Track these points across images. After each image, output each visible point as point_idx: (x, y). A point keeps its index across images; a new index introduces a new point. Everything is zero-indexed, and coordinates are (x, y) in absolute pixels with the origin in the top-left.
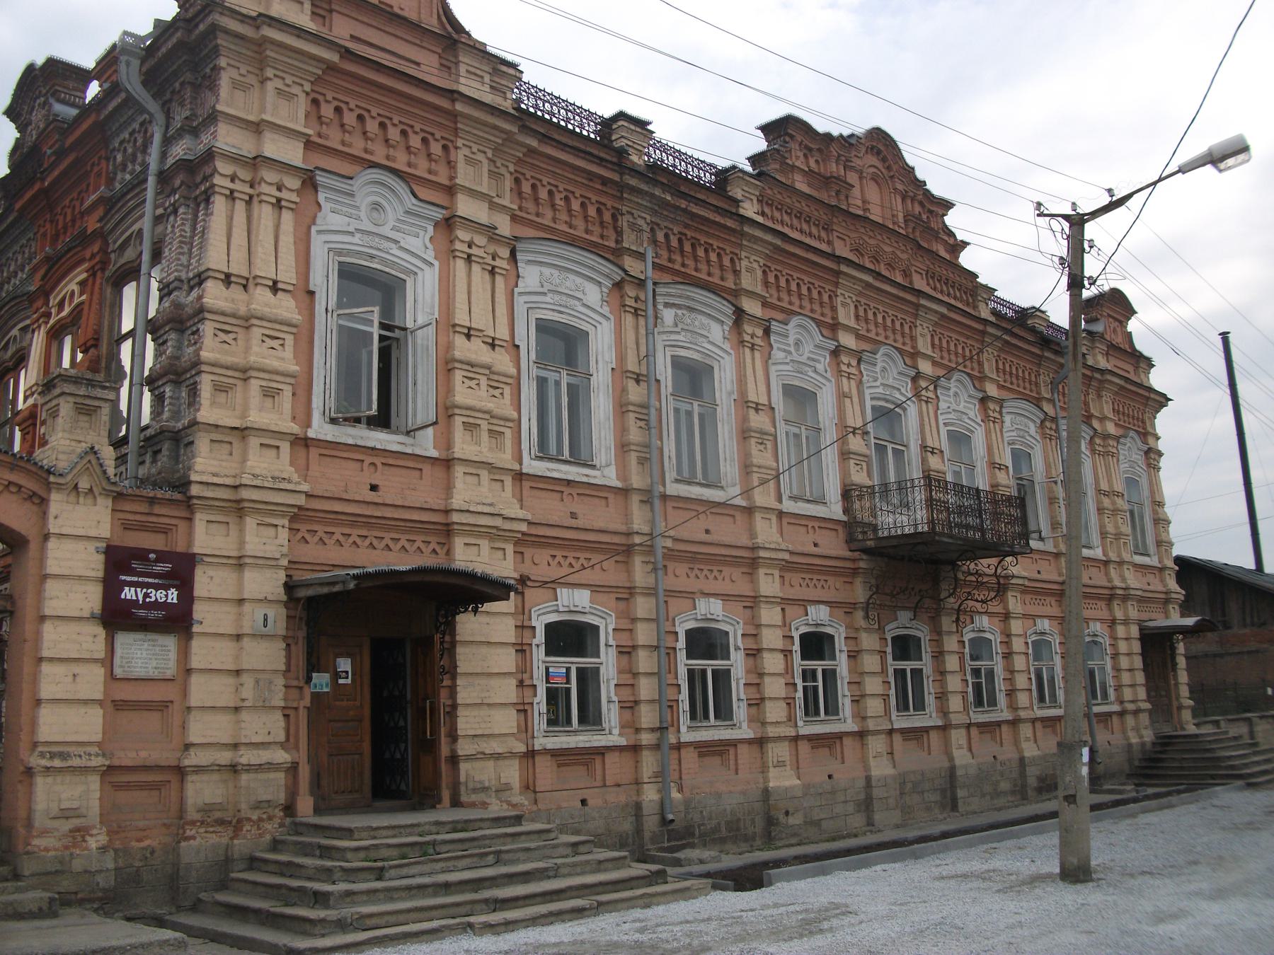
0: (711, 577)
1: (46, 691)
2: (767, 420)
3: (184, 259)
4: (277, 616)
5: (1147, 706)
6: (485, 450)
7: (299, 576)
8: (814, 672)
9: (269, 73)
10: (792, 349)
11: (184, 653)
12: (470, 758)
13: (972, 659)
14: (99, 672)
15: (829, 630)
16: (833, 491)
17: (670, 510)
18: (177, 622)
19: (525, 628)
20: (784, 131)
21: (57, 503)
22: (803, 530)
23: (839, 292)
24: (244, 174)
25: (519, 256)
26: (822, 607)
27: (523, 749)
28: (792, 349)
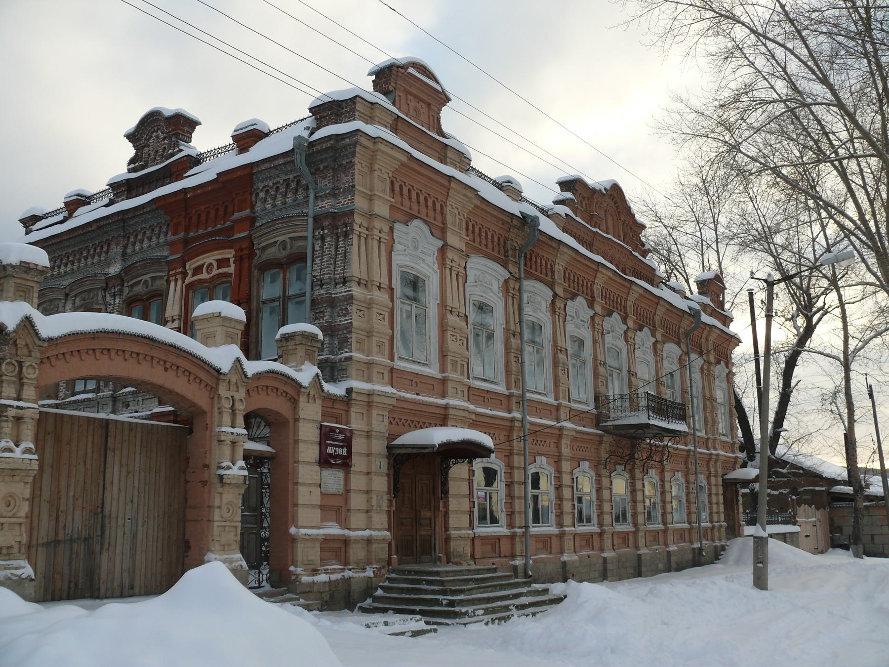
0: (406, 425)
1: (301, 500)
3: (332, 267)
4: (384, 462)
5: (725, 524)
11: (347, 481)
14: (316, 491)
18: (345, 464)
20: (570, 185)
23: (448, 203)
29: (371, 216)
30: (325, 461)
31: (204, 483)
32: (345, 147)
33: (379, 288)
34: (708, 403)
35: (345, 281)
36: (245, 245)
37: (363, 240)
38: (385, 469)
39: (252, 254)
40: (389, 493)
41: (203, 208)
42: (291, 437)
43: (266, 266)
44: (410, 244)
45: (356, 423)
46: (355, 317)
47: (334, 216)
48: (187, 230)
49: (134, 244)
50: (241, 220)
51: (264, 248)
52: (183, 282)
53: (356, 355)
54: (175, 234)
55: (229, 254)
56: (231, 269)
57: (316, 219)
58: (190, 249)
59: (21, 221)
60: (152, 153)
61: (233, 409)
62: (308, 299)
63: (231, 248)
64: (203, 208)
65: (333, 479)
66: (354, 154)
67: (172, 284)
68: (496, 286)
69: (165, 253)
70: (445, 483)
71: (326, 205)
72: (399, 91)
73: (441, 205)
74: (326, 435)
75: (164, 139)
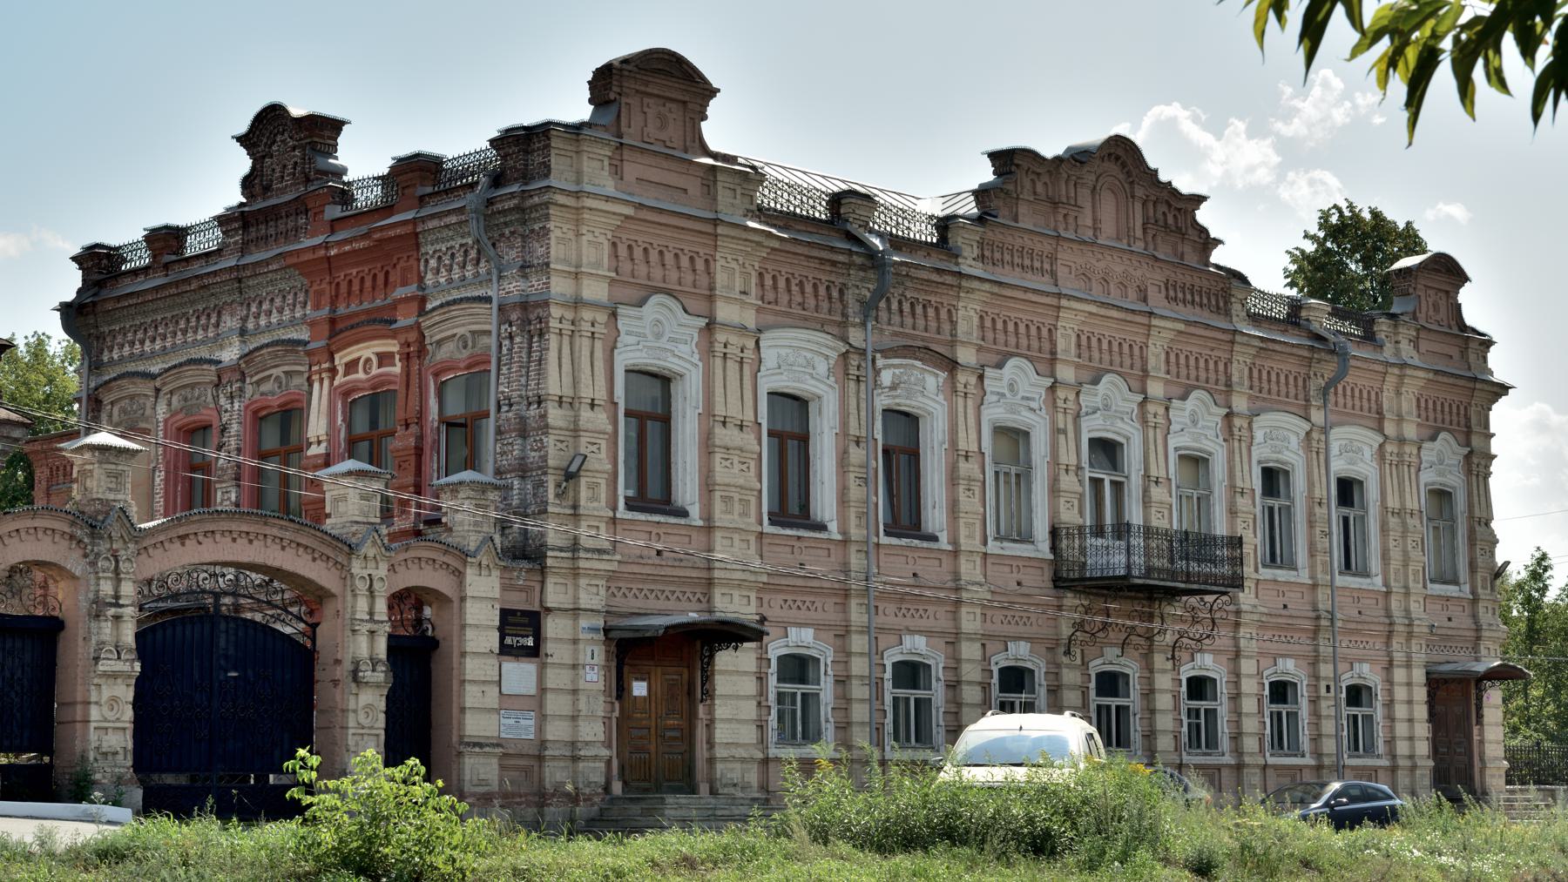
1: (469, 702)
2: (752, 436)
3: (523, 380)
6: (736, 517)
7: (614, 622)
8: (1198, 711)
9: (584, 230)
10: (1006, 391)
12: (724, 760)
13: (1190, 697)
14: (493, 691)
15: (1029, 665)
16: (1041, 531)
17: (882, 556)
19: (763, 660)
21: (470, 574)
22: (1007, 569)
24: (569, 315)
25: (762, 344)
26: (1022, 643)
27: (760, 755)
28: (1006, 391)
29: (577, 303)
31: (336, 682)
32: (535, 207)
33: (592, 405)
34: (1393, 521)
36: (412, 336)
37: (566, 340)
39: (422, 351)
41: (354, 272)
42: (456, 621)
44: (647, 332)
45: (555, 595)
49: (257, 316)
50: (407, 300)
51: (439, 343)
52: (331, 384)
54: (317, 307)
55: (392, 346)
56: (397, 369)
58: (338, 331)
59: (74, 259)
60: (278, 169)
61: (371, 590)
63: (394, 337)
64: (354, 272)
65: (520, 675)
66: (547, 217)
67: (316, 386)
68: (822, 367)
69: (305, 336)
70: (708, 677)
71: (514, 287)
72: (627, 95)
73: (707, 261)
75: (294, 148)
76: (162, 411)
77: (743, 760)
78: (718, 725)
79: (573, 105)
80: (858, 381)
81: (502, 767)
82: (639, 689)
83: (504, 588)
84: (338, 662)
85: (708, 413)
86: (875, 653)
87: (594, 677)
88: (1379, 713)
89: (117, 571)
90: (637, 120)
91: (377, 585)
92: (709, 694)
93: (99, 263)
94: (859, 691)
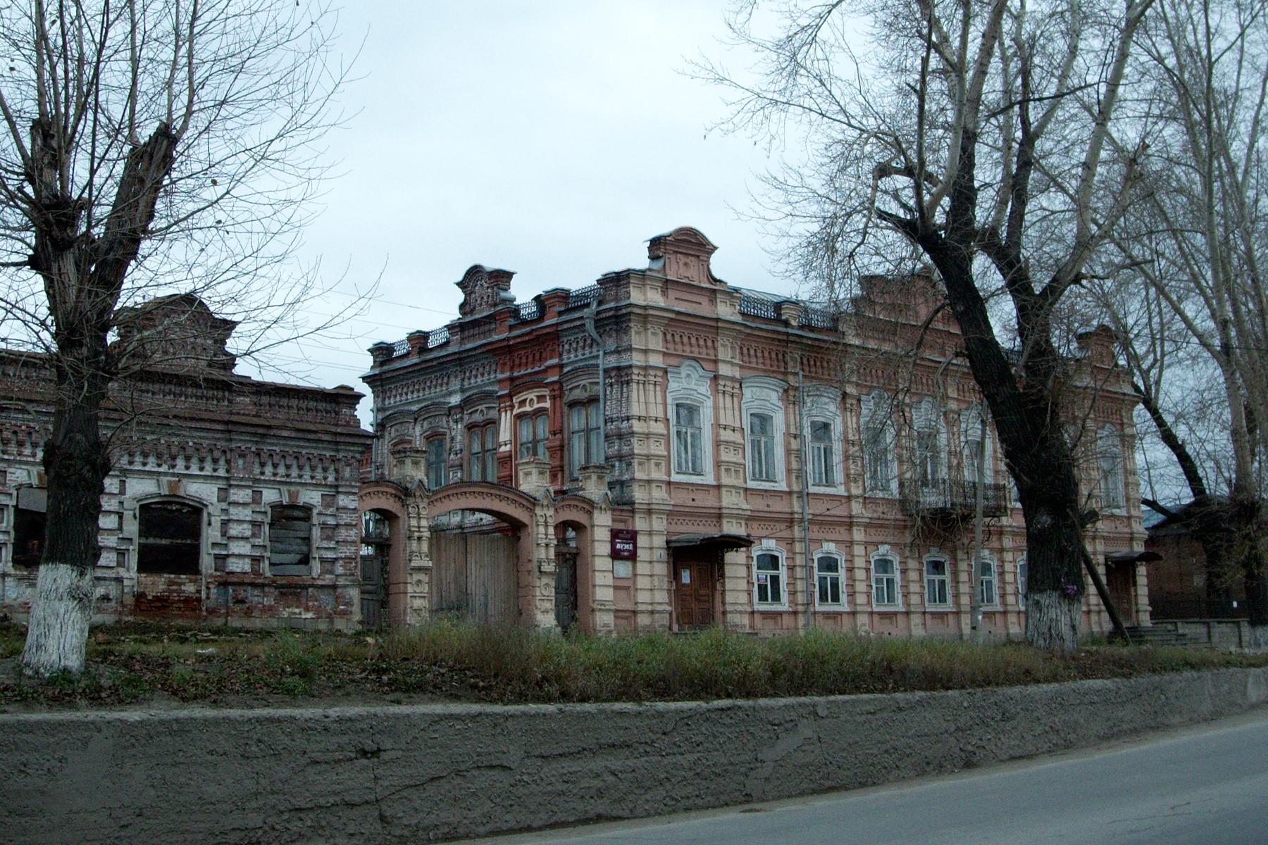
1: (598, 582)
4: (664, 553)
11: (634, 568)
12: (731, 612)
18: (632, 557)
19: (749, 557)
21: (596, 514)
30: (615, 555)
35: (628, 419)
36: (556, 387)
38: (665, 558)
40: (668, 576)
43: (573, 405)
45: (640, 524)
46: (636, 446)
47: (619, 369)
48: (512, 369)
50: (553, 366)
53: (638, 475)
55: (546, 392)
57: (606, 371)
58: (517, 385)
62: (602, 431)
65: (623, 569)
70: (722, 568)
71: (612, 361)
74: (615, 534)
76: (418, 430)
77: (741, 612)
78: (727, 593)
79: (640, 260)
80: (655, 384)
81: (616, 617)
82: (686, 577)
83: (614, 520)
84: (530, 561)
85: (717, 425)
86: (807, 553)
87: (662, 569)
88: (995, 580)
89: (419, 514)
90: (674, 266)
91: (549, 520)
92: (722, 576)
93: (382, 352)
94: (860, 574)
